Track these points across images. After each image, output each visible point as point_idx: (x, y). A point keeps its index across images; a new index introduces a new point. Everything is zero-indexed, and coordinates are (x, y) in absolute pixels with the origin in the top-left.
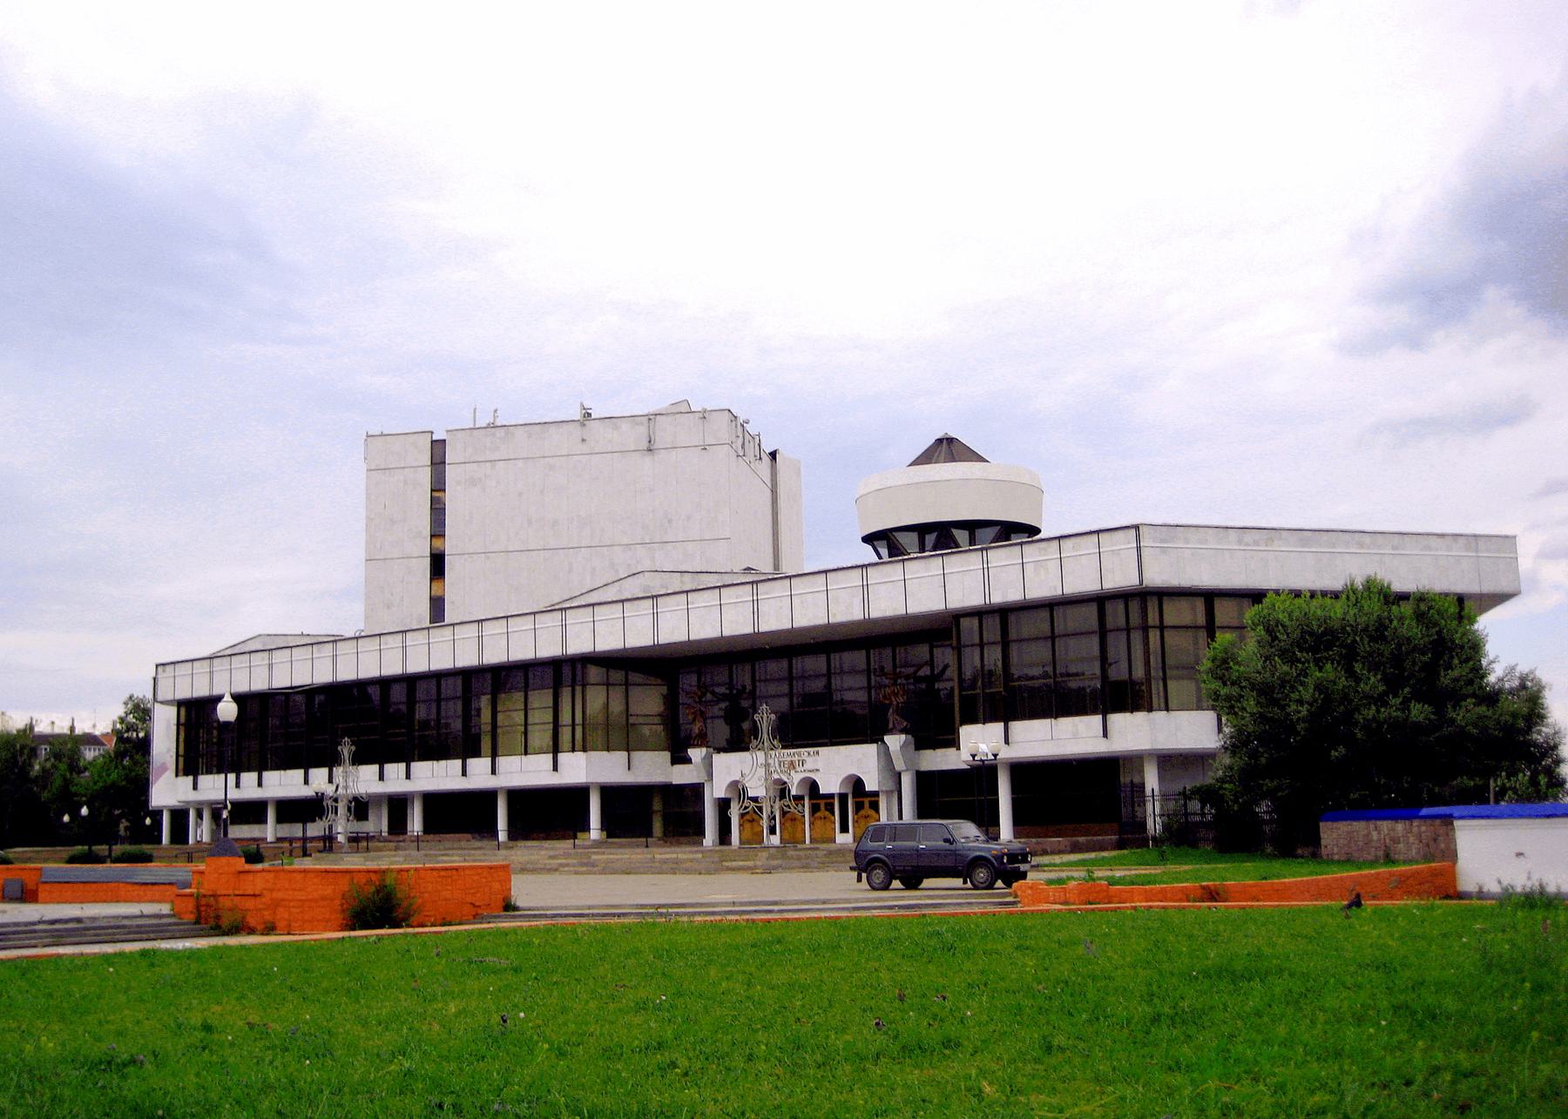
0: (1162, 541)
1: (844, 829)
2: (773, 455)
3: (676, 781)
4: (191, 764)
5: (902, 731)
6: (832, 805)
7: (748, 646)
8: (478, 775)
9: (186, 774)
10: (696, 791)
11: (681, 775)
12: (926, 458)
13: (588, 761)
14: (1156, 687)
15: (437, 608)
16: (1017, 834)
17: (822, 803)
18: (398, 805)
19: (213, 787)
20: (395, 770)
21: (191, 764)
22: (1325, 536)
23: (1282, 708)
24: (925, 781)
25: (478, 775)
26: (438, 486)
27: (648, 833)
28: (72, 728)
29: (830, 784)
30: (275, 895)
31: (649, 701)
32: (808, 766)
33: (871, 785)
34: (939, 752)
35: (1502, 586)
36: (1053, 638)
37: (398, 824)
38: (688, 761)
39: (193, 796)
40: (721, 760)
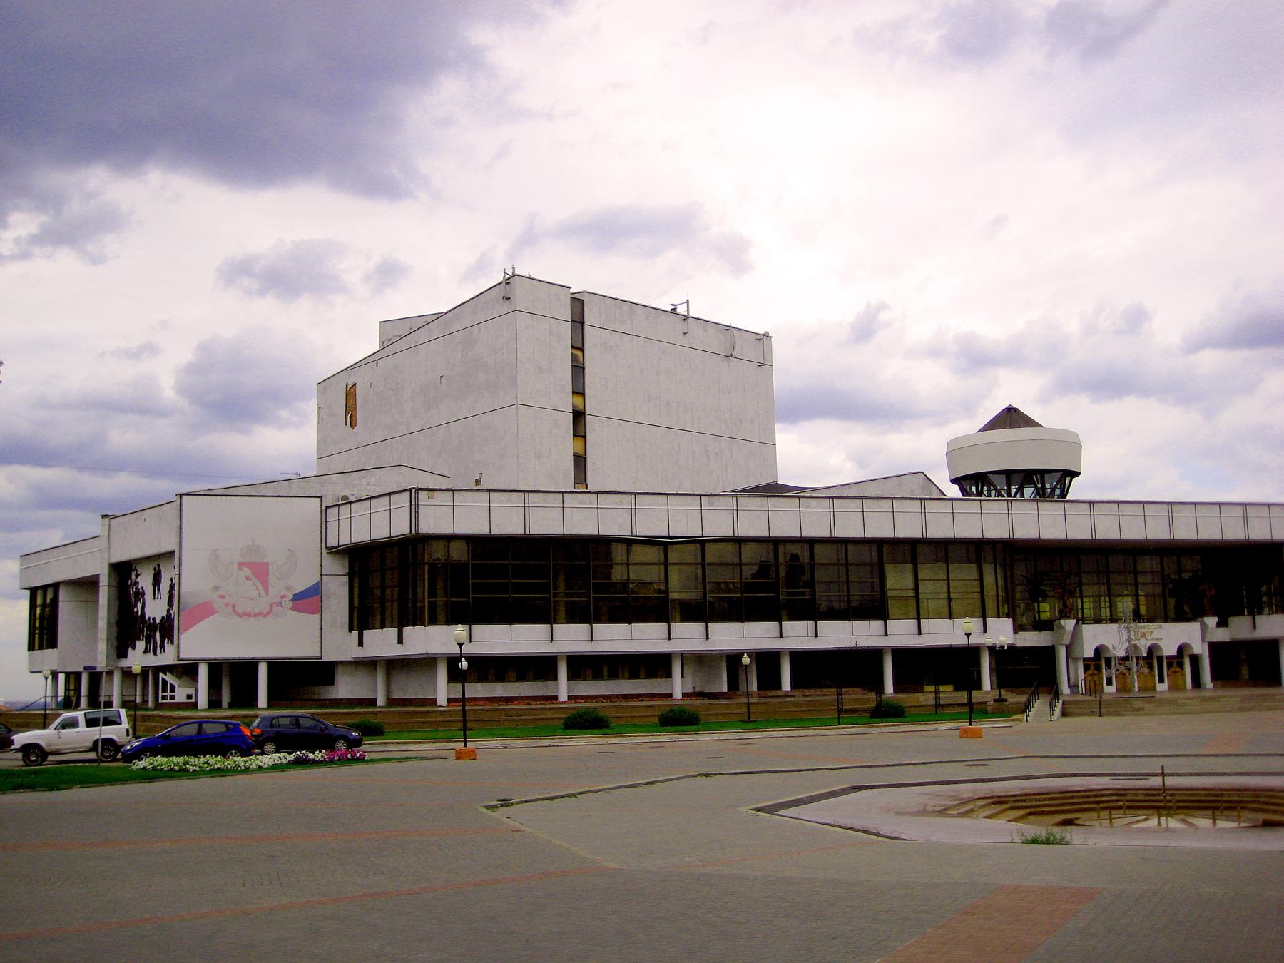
1: (1161, 681)
12: (995, 424)
16: (896, 691)
18: (767, 662)
26: (578, 347)
32: (1155, 635)
36: (628, 564)
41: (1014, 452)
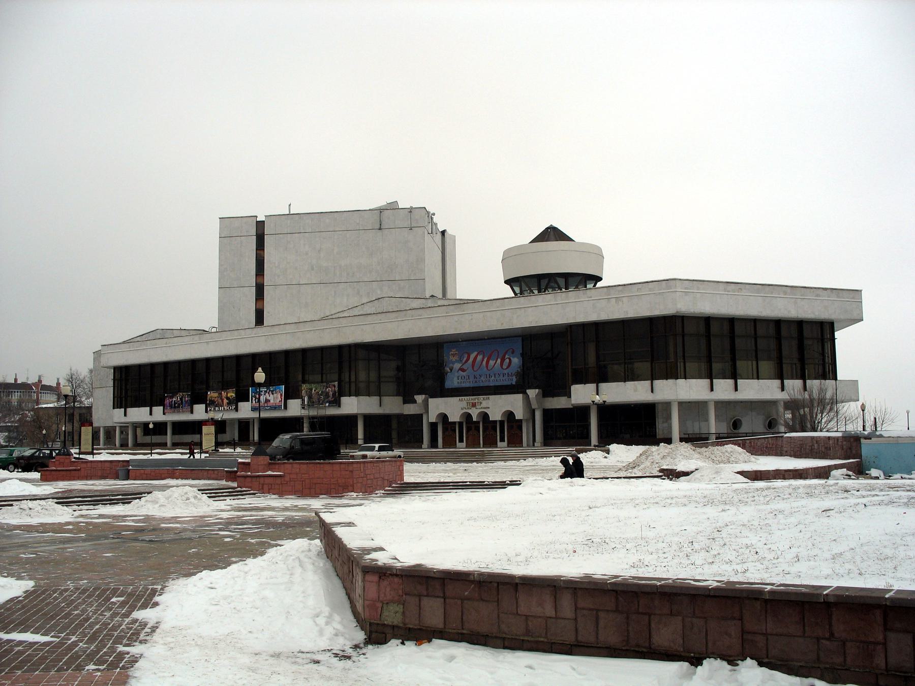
2: (443, 233)
3: (406, 413)
10: (418, 418)
11: (410, 409)
13: (358, 401)
14: (680, 365)
17: (473, 426)
22: (767, 288)
23: (304, 382)
24: (548, 414)
28: (16, 380)
29: (496, 415)
30: (292, 476)
31: (389, 369)
32: (484, 404)
33: (519, 415)
34: (555, 399)
35: (855, 316)
38: (415, 402)
39: (124, 420)
40: (433, 402)
41: (555, 260)
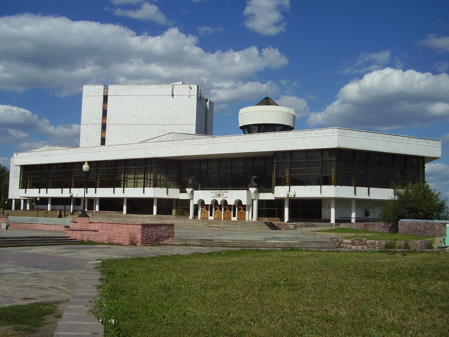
0: (343, 134)
1: (234, 216)
4: (24, 185)
5: (255, 187)
6: (208, 208)
7: (225, 157)
8: (118, 193)
9: (23, 188)
15: (103, 142)
18: (91, 201)
19: (33, 193)
20: (43, 191)
21: (24, 185)
25: (118, 193)
27: (171, 214)
29: (231, 202)
32: (225, 195)
33: (244, 203)
37: (91, 207)
